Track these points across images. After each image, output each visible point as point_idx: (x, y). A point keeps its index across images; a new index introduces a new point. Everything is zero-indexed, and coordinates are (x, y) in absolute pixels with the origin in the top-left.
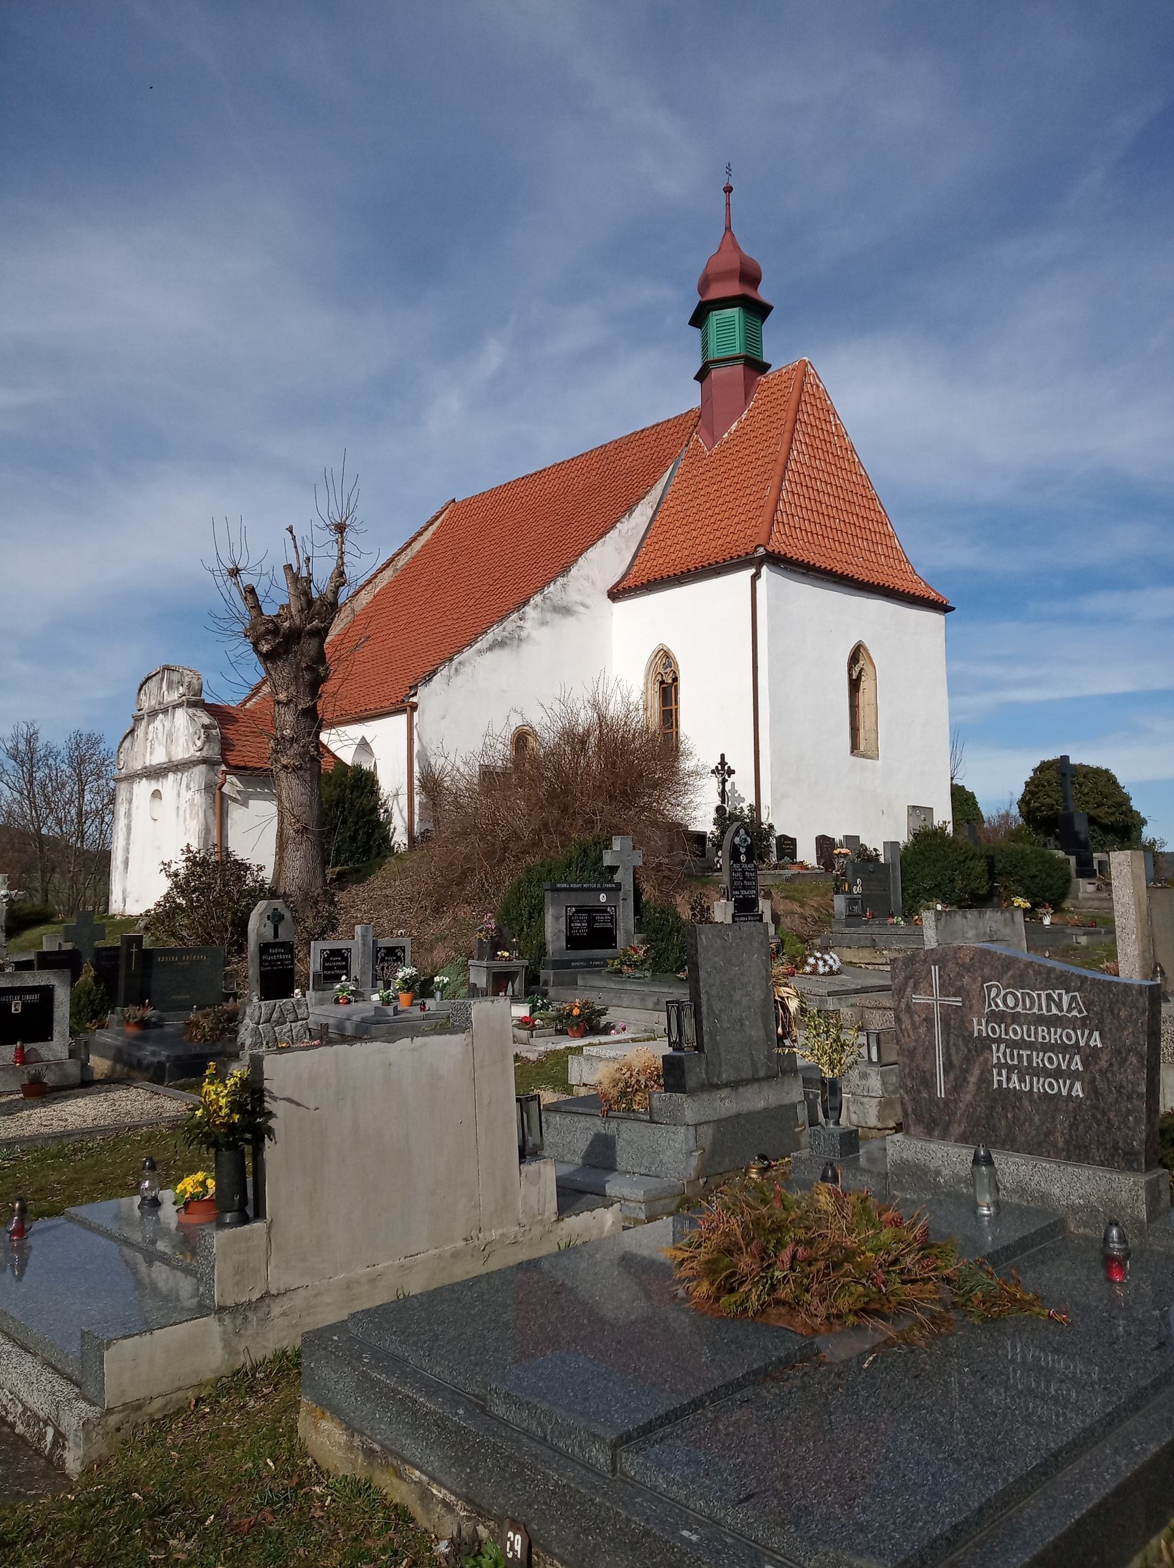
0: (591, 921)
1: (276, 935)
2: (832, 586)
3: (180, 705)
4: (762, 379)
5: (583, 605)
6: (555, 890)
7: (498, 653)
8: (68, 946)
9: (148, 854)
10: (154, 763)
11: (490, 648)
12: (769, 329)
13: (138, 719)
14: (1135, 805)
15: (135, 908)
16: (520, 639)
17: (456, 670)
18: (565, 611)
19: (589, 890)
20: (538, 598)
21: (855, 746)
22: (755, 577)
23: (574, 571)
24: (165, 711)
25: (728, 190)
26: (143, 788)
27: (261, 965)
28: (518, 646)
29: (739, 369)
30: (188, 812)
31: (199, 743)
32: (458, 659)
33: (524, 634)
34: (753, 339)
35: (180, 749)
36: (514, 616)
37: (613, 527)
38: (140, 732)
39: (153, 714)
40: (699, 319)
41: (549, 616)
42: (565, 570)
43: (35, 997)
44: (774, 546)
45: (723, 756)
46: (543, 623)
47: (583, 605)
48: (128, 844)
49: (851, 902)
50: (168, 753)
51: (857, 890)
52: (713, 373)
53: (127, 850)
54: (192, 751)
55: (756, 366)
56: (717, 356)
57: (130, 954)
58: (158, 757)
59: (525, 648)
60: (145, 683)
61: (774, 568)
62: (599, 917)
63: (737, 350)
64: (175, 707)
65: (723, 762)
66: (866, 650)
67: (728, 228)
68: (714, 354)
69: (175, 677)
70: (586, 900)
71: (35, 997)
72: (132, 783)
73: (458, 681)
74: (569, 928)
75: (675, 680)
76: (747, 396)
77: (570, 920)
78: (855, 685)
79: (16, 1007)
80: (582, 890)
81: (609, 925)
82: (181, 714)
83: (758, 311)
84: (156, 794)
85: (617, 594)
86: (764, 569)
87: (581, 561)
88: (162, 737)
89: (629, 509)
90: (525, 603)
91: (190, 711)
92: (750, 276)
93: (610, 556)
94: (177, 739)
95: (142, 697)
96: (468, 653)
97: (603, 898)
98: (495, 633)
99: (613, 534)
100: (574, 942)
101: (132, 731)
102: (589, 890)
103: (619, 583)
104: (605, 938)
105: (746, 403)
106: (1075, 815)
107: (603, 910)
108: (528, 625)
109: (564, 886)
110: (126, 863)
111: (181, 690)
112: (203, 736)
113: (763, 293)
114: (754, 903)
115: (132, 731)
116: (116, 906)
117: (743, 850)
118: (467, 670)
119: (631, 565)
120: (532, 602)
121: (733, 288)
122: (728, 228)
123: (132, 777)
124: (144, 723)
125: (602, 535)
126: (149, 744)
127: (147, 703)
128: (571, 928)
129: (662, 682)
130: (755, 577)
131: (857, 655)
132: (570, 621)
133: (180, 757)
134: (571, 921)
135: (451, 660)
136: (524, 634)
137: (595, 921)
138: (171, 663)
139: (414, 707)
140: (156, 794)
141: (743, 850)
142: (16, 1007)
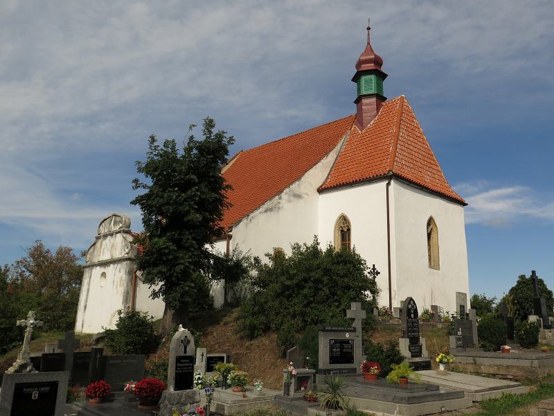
0: (342, 348)
1: (185, 352)
2: (419, 191)
3: (120, 232)
4: (384, 104)
5: (307, 194)
6: (324, 330)
7: (268, 213)
8: (58, 351)
9: (101, 306)
10: (104, 259)
11: (266, 211)
12: (385, 83)
13: (98, 238)
14: (514, 284)
15: (88, 330)
16: (279, 208)
17: (250, 220)
18: (298, 196)
19: (341, 331)
20: (287, 190)
21: (430, 264)
22: (388, 184)
23: (303, 179)
24: (111, 235)
25: (369, 29)
26: (97, 271)
27: (176, 369)
28: (278, 211)
29: (374, 100)
30: (119, 283)
31: (127, 250)
32: (251, 215)
33: (281, 206)
34: (379, 87)
35: (117, 253)
36: (277, 197)
37: (319, 161)
38: (98, 244)
39: (105, 236)
40: (356, 79)
41: (292, 198)
42: (299, 178)
43: (47, 389)
44: (396, 170)
45: (374, 265)
46: (289, 201)
47: (307, 194)
48: (87, 298)
49: (458, 339)
50: (112, 255)
51: (460, 333)
52: (363, 100)
53: (86, 301)
54: (123, 254)
55: (380, 98)
56: (364, 93)
57: (96, 358)
58: (106, 257)
59: (280, 211)
60: (103, 222)
61: (397, 182)
62: (345, 346)
63: (373, 91)
64: (117, 233)
65: (374, 269)
66: (433, 220)
67: (369, 44)
68: (364, 92)
69: (118, 219)
70: (339, 337)
71: (47, 389)
72: (92, 269)
73: (251, 226)
74: (331, 352)
75: (349, 230)
76: (378, 109)
77: (332, 347)
78: (429, 235)
79: (35, 395)
80: (337, 331)
81: (350, 350)
82: (119, 235)
83: (382, 76)
84: (104, 275)
85: (321, 190)
86: (392, 182)
87: (306, 174)
88: (109, 246)
89: (326, 154)
90: (281, 192)
91: (125, 235)
92: (378, 62)
93: (318, 174)
94: (117, 248)
95: (101, 228)
96: (256, 213)
97: (347, 335)
98: (268, 205)
99: (320, 164)
100: (333, 360)
101: (94, 244)
102: (341, 331)
103: (322, 186)
104: (348, 358)
105: (378, 113)
106: (529, 292)
107: (347, 342)
108: (283, 201)
109: (329, 328)
110: (85, 307)
111: (121, 225)
112: (129, 247)
113: (383, 69)
114: (418, 339)
115: (94, 244)
116: (78, 328)
117: (412, 312)
118: (254, 221)
119: (327, 178)
120: (285, 191)
121: (371, 66)
122: (369, 44)
123: (93, 266)
124: (100, 241)
125: (315, 164)
126: (102, 250)
127: (104, 230)
128: (332, 351)
129: (342, 231)
130: (388, 184)
131: (431, 222)
132: (301, 201)
133: (117, 257)
134: (332, 348)
135: (248, 215)
136: (281, 206)
137: (343, 348)
138: (117, 213)
139: (230, 237)
140: (104, 275)
141: (412, 312)
142: (35, 395)
